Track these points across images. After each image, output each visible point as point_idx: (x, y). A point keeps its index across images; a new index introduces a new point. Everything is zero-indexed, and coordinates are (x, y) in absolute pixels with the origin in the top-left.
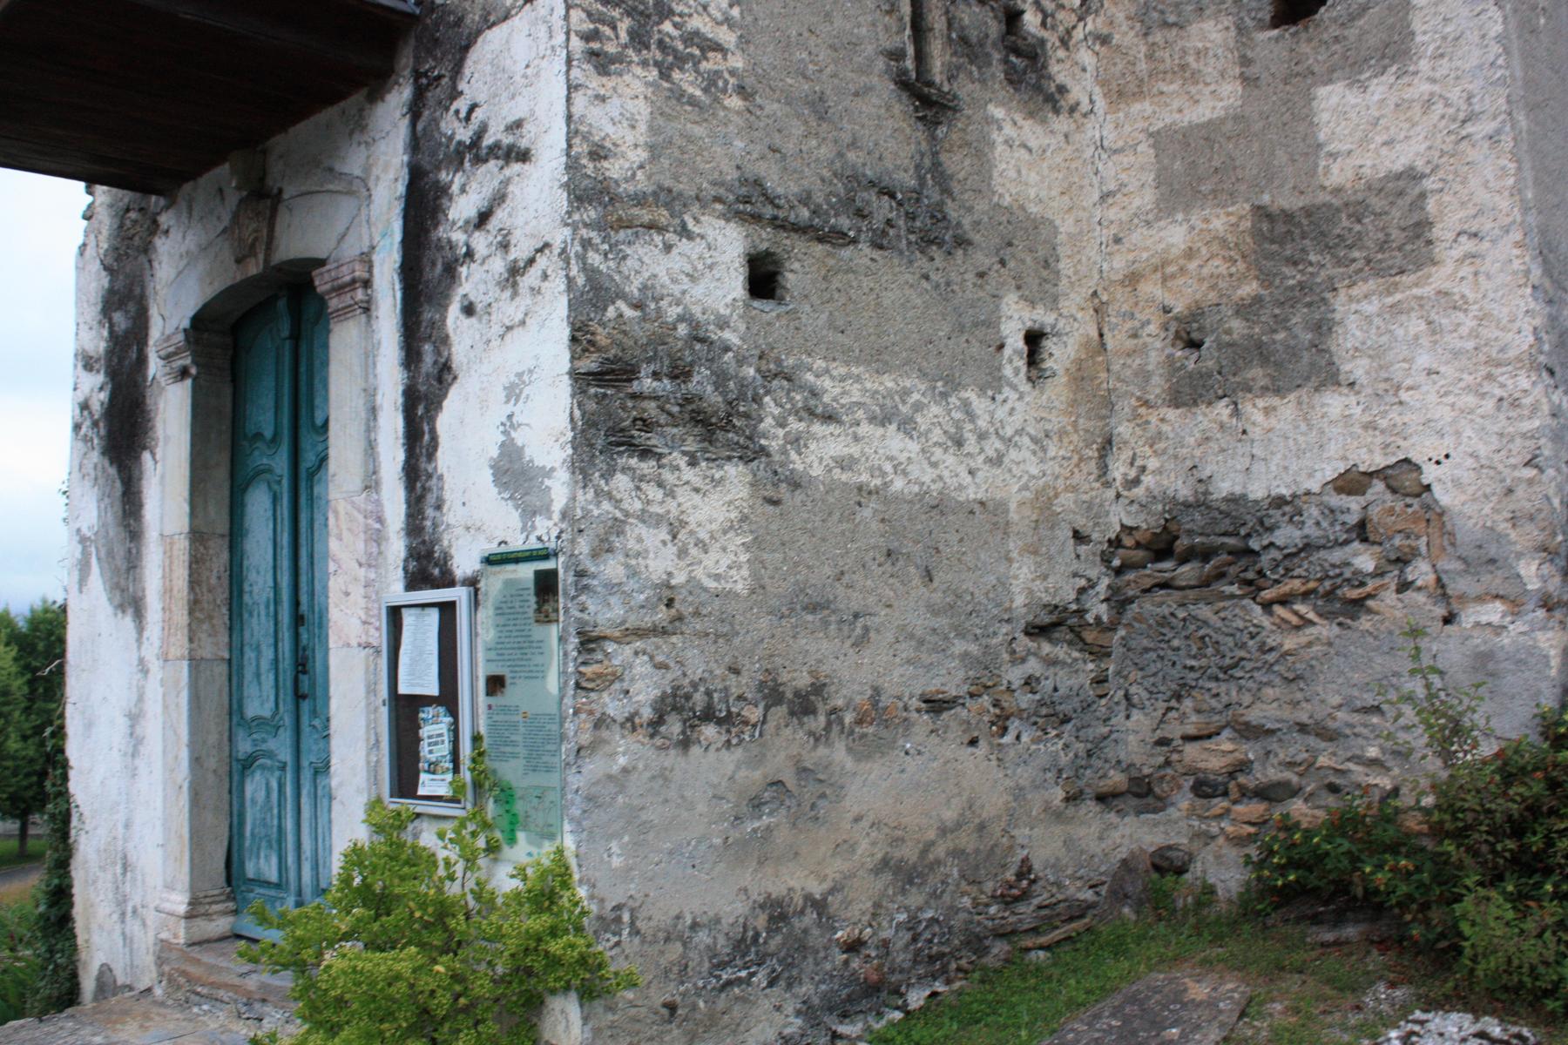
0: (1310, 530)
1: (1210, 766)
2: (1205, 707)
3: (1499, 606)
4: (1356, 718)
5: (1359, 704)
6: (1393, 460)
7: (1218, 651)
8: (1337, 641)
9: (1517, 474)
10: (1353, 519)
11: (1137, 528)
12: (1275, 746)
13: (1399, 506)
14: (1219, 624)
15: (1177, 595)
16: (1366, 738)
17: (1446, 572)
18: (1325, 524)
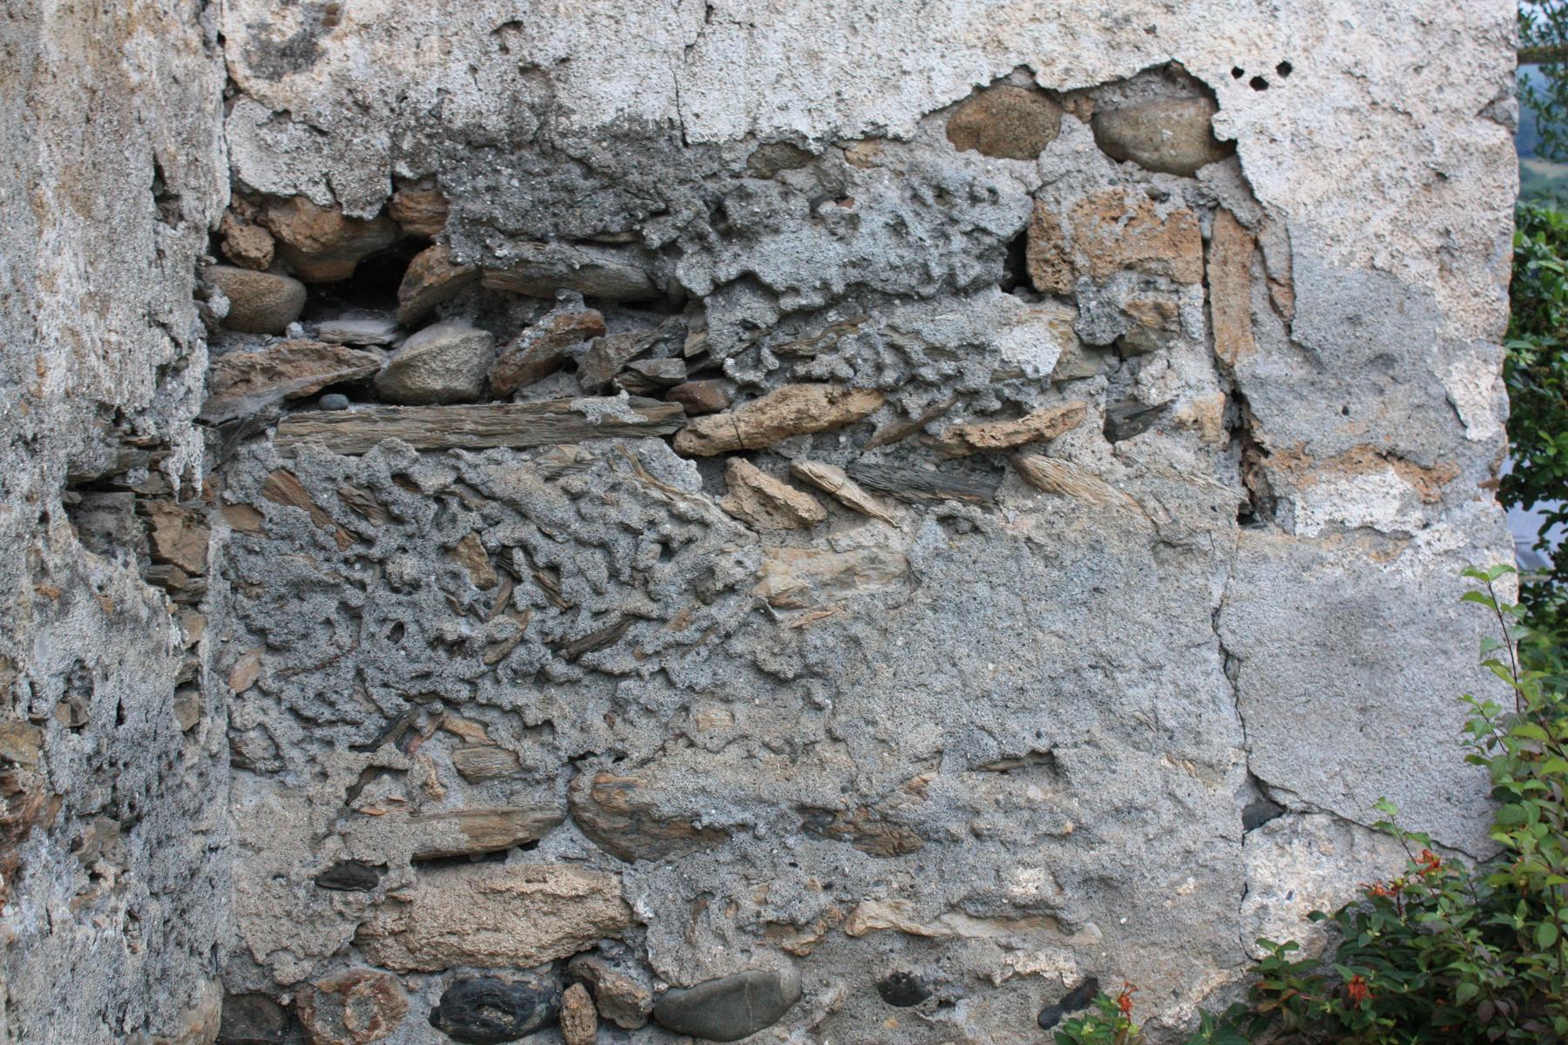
0: (873, 242)
1: (507, 943)
2: (498, 762)
3: (1393, 478)
4: (982, 788)
5: (992, 749)
6: (1131, 65)
7: (553, 594)
8: (938, 567)
9: (1460, 133)
10: (1004, 222)
11: (287, 202)
12: (727, 878)
13: (1135, 197)
14: (563, 510)
15: (416, 420)
16: (1010, 845)
17: (1262, 383)
18: (918, 230)
